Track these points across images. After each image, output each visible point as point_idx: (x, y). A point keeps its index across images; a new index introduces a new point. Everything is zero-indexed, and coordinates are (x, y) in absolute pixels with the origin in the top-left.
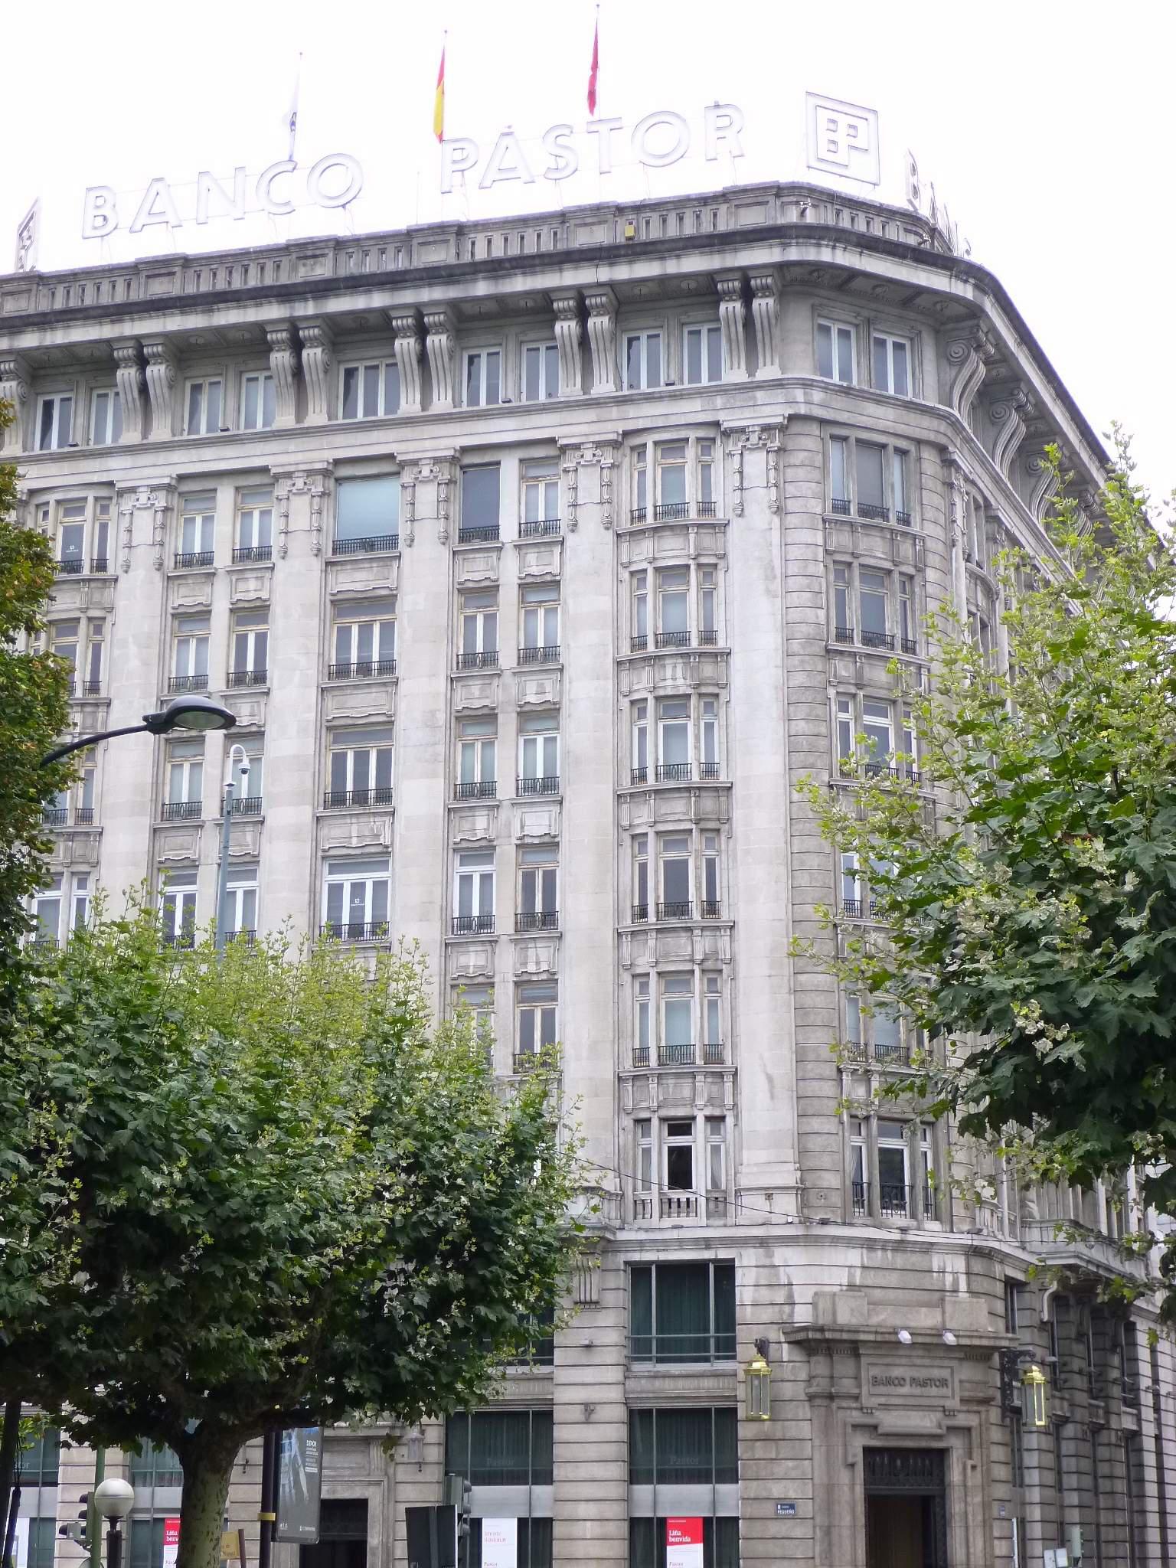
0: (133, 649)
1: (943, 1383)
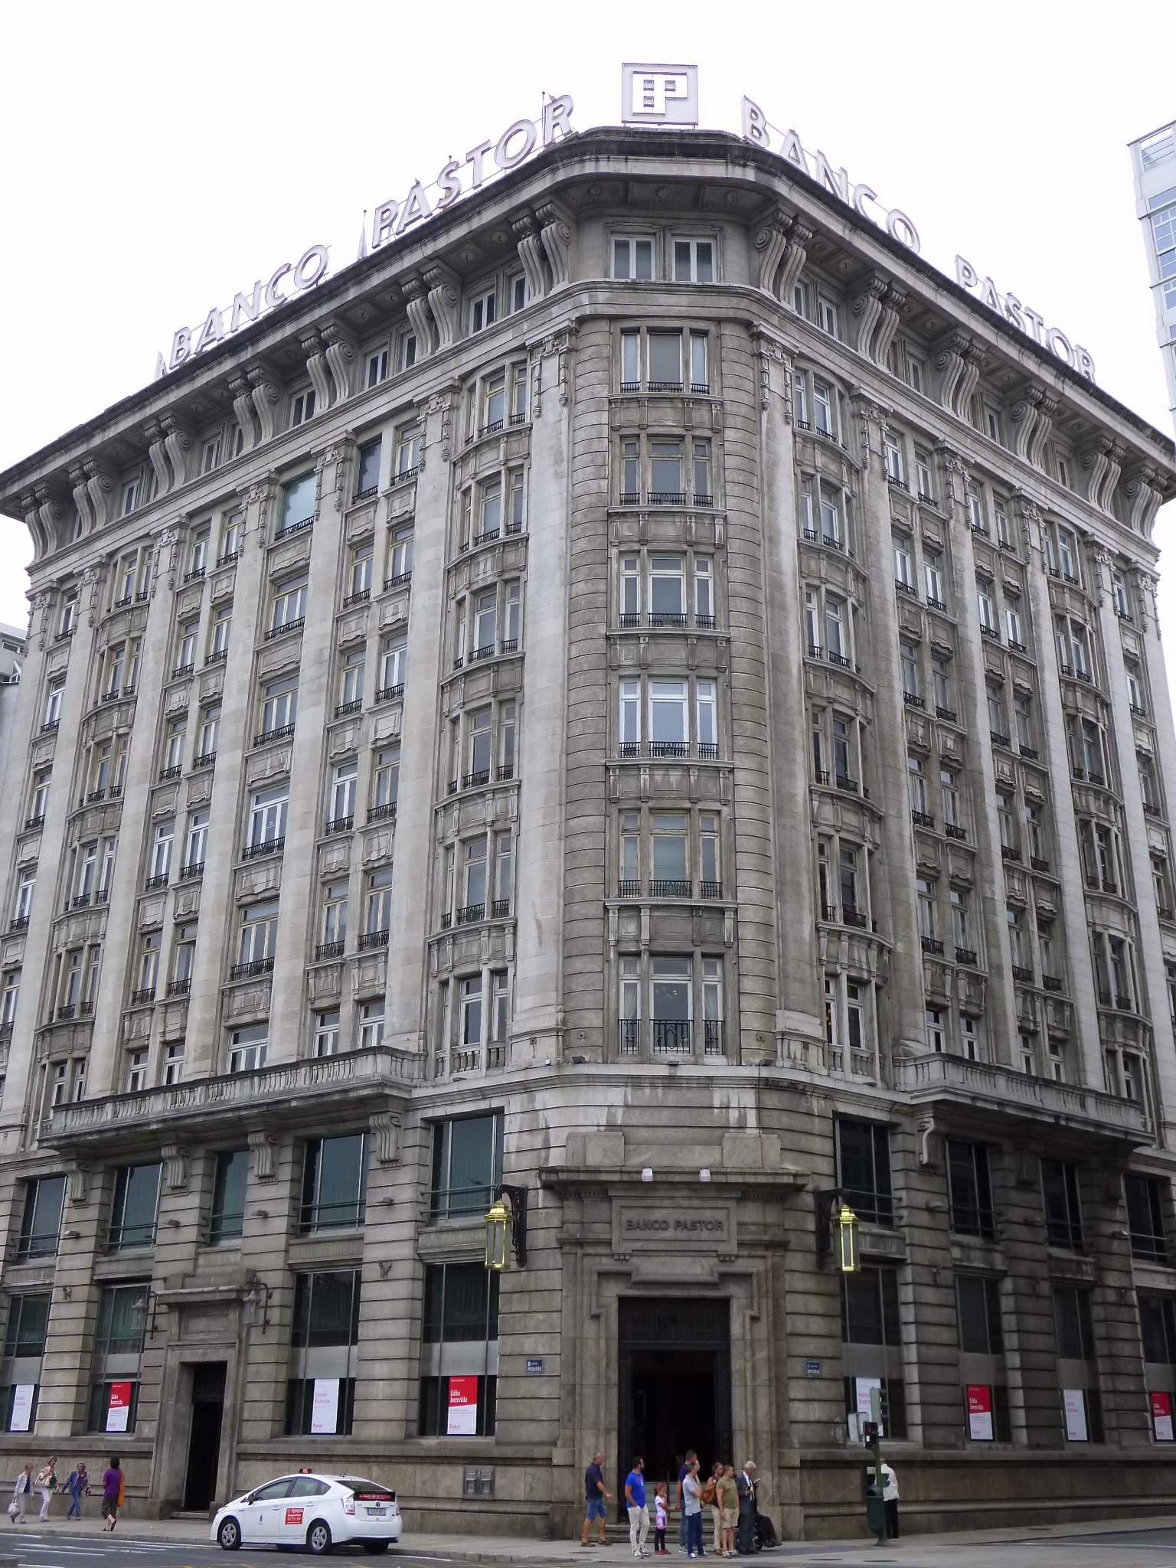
0: (151, 653)
1: (718, 1225)
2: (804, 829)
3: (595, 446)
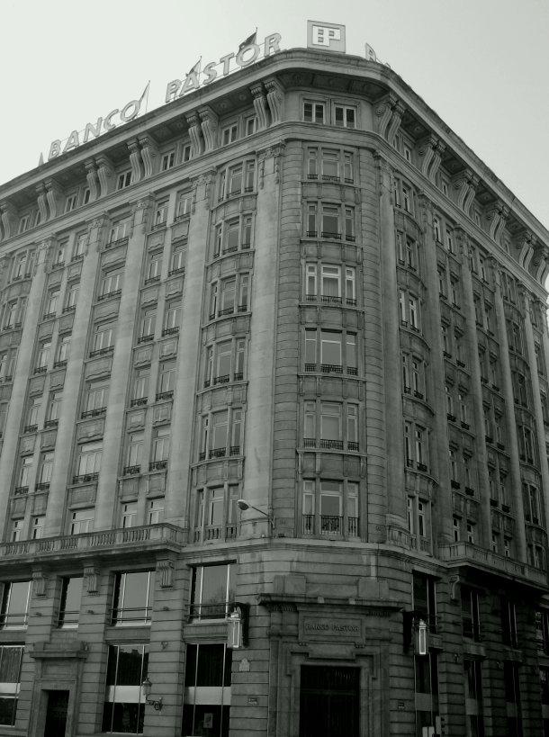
0: (32, 305)
2: (399, 414)
3: (294, 205)
